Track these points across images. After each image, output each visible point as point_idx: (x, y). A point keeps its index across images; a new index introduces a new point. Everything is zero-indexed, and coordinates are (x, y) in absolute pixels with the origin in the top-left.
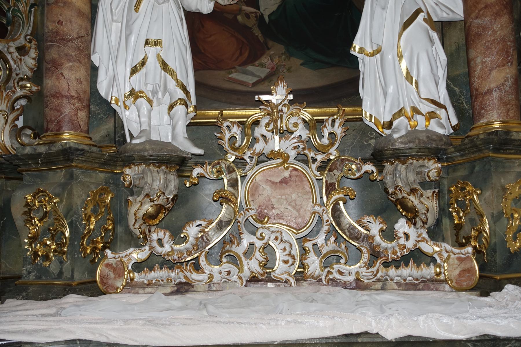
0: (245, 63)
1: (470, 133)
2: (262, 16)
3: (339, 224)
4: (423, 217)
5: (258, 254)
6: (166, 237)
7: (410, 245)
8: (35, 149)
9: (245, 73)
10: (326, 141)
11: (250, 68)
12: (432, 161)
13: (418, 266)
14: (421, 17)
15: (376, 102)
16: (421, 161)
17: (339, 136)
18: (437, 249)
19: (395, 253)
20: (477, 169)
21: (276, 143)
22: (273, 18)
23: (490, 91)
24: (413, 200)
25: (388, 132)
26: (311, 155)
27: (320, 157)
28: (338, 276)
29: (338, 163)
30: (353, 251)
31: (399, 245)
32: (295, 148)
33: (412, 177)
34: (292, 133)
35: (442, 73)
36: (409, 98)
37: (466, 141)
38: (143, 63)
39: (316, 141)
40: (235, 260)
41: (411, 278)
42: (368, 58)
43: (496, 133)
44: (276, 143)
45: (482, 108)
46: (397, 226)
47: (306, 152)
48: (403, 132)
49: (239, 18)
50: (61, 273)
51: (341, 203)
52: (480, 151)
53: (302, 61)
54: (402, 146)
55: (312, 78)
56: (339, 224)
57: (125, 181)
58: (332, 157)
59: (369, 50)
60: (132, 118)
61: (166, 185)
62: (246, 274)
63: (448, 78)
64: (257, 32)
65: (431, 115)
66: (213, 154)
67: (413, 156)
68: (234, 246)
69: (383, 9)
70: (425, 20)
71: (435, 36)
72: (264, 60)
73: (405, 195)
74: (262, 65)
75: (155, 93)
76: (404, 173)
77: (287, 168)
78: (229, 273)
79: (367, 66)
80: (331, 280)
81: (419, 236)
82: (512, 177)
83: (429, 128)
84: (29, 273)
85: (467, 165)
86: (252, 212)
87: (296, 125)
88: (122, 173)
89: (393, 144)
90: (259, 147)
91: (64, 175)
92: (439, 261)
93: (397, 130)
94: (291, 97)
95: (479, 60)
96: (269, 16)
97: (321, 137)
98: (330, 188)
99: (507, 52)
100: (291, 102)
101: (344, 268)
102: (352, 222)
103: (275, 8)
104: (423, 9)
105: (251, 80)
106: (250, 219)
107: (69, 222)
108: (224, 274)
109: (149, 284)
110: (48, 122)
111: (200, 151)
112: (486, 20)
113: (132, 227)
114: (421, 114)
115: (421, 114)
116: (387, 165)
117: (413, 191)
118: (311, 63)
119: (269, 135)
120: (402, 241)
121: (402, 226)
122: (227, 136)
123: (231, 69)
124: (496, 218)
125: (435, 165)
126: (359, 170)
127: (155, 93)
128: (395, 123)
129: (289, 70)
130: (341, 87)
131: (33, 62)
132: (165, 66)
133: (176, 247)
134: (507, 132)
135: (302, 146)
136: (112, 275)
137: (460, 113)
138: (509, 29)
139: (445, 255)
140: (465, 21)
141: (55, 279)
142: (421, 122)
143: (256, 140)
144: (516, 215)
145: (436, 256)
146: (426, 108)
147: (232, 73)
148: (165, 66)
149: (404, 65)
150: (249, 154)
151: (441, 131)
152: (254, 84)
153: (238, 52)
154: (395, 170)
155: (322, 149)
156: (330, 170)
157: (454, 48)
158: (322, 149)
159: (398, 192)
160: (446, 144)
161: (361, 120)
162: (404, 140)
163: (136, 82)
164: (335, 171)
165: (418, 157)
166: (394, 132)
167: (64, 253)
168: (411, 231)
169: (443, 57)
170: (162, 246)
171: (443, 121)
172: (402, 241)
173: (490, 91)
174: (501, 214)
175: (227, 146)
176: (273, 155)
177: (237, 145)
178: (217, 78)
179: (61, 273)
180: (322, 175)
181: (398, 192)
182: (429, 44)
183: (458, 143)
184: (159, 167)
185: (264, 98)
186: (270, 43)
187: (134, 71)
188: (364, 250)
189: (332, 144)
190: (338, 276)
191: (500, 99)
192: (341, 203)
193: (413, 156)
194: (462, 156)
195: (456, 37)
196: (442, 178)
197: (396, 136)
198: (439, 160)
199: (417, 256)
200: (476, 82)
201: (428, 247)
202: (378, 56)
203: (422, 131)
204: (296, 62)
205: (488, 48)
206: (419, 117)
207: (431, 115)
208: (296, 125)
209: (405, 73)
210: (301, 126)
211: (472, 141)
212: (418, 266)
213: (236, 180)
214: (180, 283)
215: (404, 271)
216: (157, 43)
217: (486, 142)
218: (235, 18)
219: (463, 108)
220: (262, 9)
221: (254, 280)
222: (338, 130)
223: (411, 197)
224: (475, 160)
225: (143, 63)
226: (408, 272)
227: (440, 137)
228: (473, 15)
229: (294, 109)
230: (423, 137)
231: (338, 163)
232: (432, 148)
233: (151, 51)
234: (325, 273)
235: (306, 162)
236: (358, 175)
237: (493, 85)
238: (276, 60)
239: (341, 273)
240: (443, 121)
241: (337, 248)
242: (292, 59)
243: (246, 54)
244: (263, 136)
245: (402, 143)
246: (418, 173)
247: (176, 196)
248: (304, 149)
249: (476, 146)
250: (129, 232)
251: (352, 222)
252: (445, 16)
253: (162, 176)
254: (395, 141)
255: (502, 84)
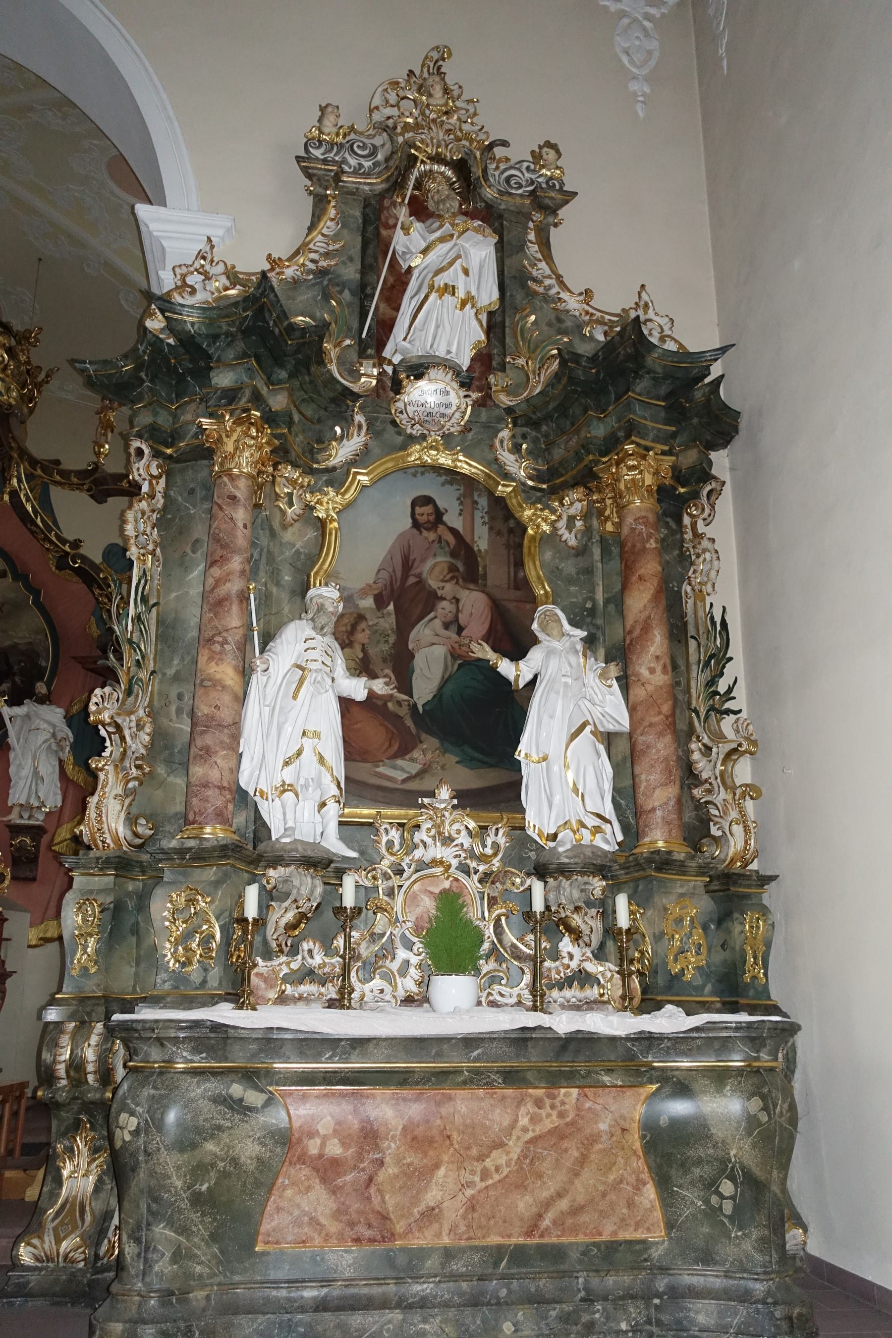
0: (395, 756)
1: (635, 851)
2: (415, 705)
3: (500, 941)
4: (586, 939)
5: (413, 971)
6: (316, 949)
7: (574, 964)
8: (183, 843)
9: (394, 767)
10: (489, 851)
11: (399, 762)
12: (597, 879)
13: (582, 987)
14: (588, 729)
15: (540, 812)
16: (586, 878)
17: (502, 846)
18: (601, 969)
19: (558, 973)
20: (641, 888)
21: (438, 851)
22: (427, 708)
23: (653, 810)
24: (577, 920)
25: (551, 844)
26: (473, 864)
27: (482, 868)
28: (499, 998)
29: (501, 875)
30: (514, 972)
31: (563, 965)
32: (456, 856)
33: (576, 894)
34: (453, 840)
35: (608, 786)
36: (574, 810)
37: (631, 859)
38: (299, 753)
39: (478, 850)
40: (388, 977)
41: (574, 1000)
42: (532, 765)
43: (658, 852)
44: (438, 851)
45: (646, 826)
46: (561, 945)
47: (468, 861)
48: (568, 846)
49: (390, 705)
50: (204, 982)
51: (503, 918)
52: (644, 869)
53: (458, 759)
54: (566, 860)
55: (472, 779)
56: (500, 941)
57: (268, 883)
58: (495, 869)
59: (535, 757)
60: (274, 814)
61: (312, 891)
62: (401, 994)
63: (615, 789)
64: (409, 723)
65: (597, 830)
66: (367, 861)
67: (578, 872)
68: (388, 962)
69: (551, 717)
70: (592, 732)
71: (601, 748)
72: (416, 754)
73: (568, 913)
74: (413, 760)
75: (306, 786)
76: (568, 890)
77: (447, 878)
78: (382, 991)
79: (532, 775)
80: (491, 1002)
81: (583, 955)
82: (673, 897)
83: (595, 843)
84: (165, 982)
85: (631, 884)
86: (409, 925)
87: (459, 832)
88: (264, 875)
89: (558, 858)
90: (418, 853)
91: (215, 874)
92: (602, 982)
93: (562, 843)
94: (455, 801)
95: (643, 777)
96: (423, 706)
97: (484, 846)
98: (493, 902)
99: (670, 771)
100: (454, 807)
101: (505, 990)
102: (515, 941)
103: (430, 697)
104: (591, 721)
105: (400, 776)
106: (407, 933)
107: (225, 925)
108: (376, 992)
109: (300, 998)
110: (195, 813)
111: (354, 854)
112: (650, 738)
113: (269, 937)
114: (587, 828)
115: (587, 828)
116: (551, 880)
117: (577, 909)
118: (467, 761)
119: (429, 841)
120: (566, 961)
121: (566, 945)
122: (384, 839)
123: (377, 762)
124: (658, 938)
125: (600, 883)
126: (522, 884)
127: (306, 786)
128: (560, 836)
129: (443, 768)
130: (498, 793)
131: (147, 738)
132: (322, 760)
133: (327, 960)
134: (669, 853)
135: (463, 855)
136: (263, 985)
137: (625, 828)
138: (672, 749)
139: (609, 975)
140: (631, 735)
141: (197, 989)
142: (586, 836)
143: (416, 846)
144: (677, 936)
145: (600, 977)
146: (592, 821)
147: (378, 766)
148: (322, 760)
149: (570, 776)
150: (407, 860)
151: (606, 847)
152: (404, 781)
153: (387, 744)
154: (559, 886)
155: (483, 858)
156: (493, 883)
157: (620, 757)
158: (483, 858)
159: (561, 910)
160: (611, 861)
161: (523, 828)
162: (570, 854)
163: (288, 775)
164: (498, 884)
165: (583, 874)
166: (559, 845)
167: (211, 958)
168: (576, 951)
169: (609, 770)
170: (312, 957)
171: (609, 836)
172: (566, 961)
173: (653, 810)
174: (662, 934)
175: (383, 850)
176: (435, 863)
177: (395, 850)
178: (363, 771)
179: (204, 982)
180: (484, 887)
181: (561, 910)
182: (595, 757)
183: (622, 860)
184: (308, 869)
185: (426, 801)
186: (424, 736)
187: (287, 763)
188: (527, 970)
189: (495, 854)
190: (499, 998)
191: (663, 818)
192: (503, 918)
193: (578, 872)
194: (626, 874)
195: (622, 747)
196: (606, 897)
197: (561, 849)
198: (604, 878)
199: (583, 978)
200: (641, 799)
201: (592, 967)
202: (544, 763)
203: (587, 846)
204: (451, 759)
205: (652, 766)
206: (584, 831)
207: (597, 830)
208: (459, 832)
209: (571, 785)
210: (464, 833)
211: (636, 859)
212: (582, 987)
213: (393, 888)
214: (331, 999)
215: (568, 993)
216: (317, 735)
217: (649, 861)
218: (385, 704)
219: (629, 824)
220: (415, 697)
221: (409, 1000)
222: (502, 840)
223: (575, 916)
224: (638, 879)
225: (299, 753)
226: (572, 994)
227: (606, 853)
228: (639, 731)
229: (457, 813)
230: (588, 852)
231: (501, 875)
232: (599, 866)
233: (308, 743)
234: (485, 995)
235: (468, 873)
236: (522, 889)
237: (657, 804)
238: (429, 755)
239: (502, 995)
240: (609, 836)
241: (498, 968)
242: (447, 755)
243: (395, 747)
244: (422, 841)
245: (567, 857)
246: (582, 891)
247: (319, 905)
248: (465, 858)
249: (639, 864)
250: (265, 942)
251: (515, 941)
252: (611, 727)
253: (309, 879)
254: (560, 854)
255: (665, 804)
